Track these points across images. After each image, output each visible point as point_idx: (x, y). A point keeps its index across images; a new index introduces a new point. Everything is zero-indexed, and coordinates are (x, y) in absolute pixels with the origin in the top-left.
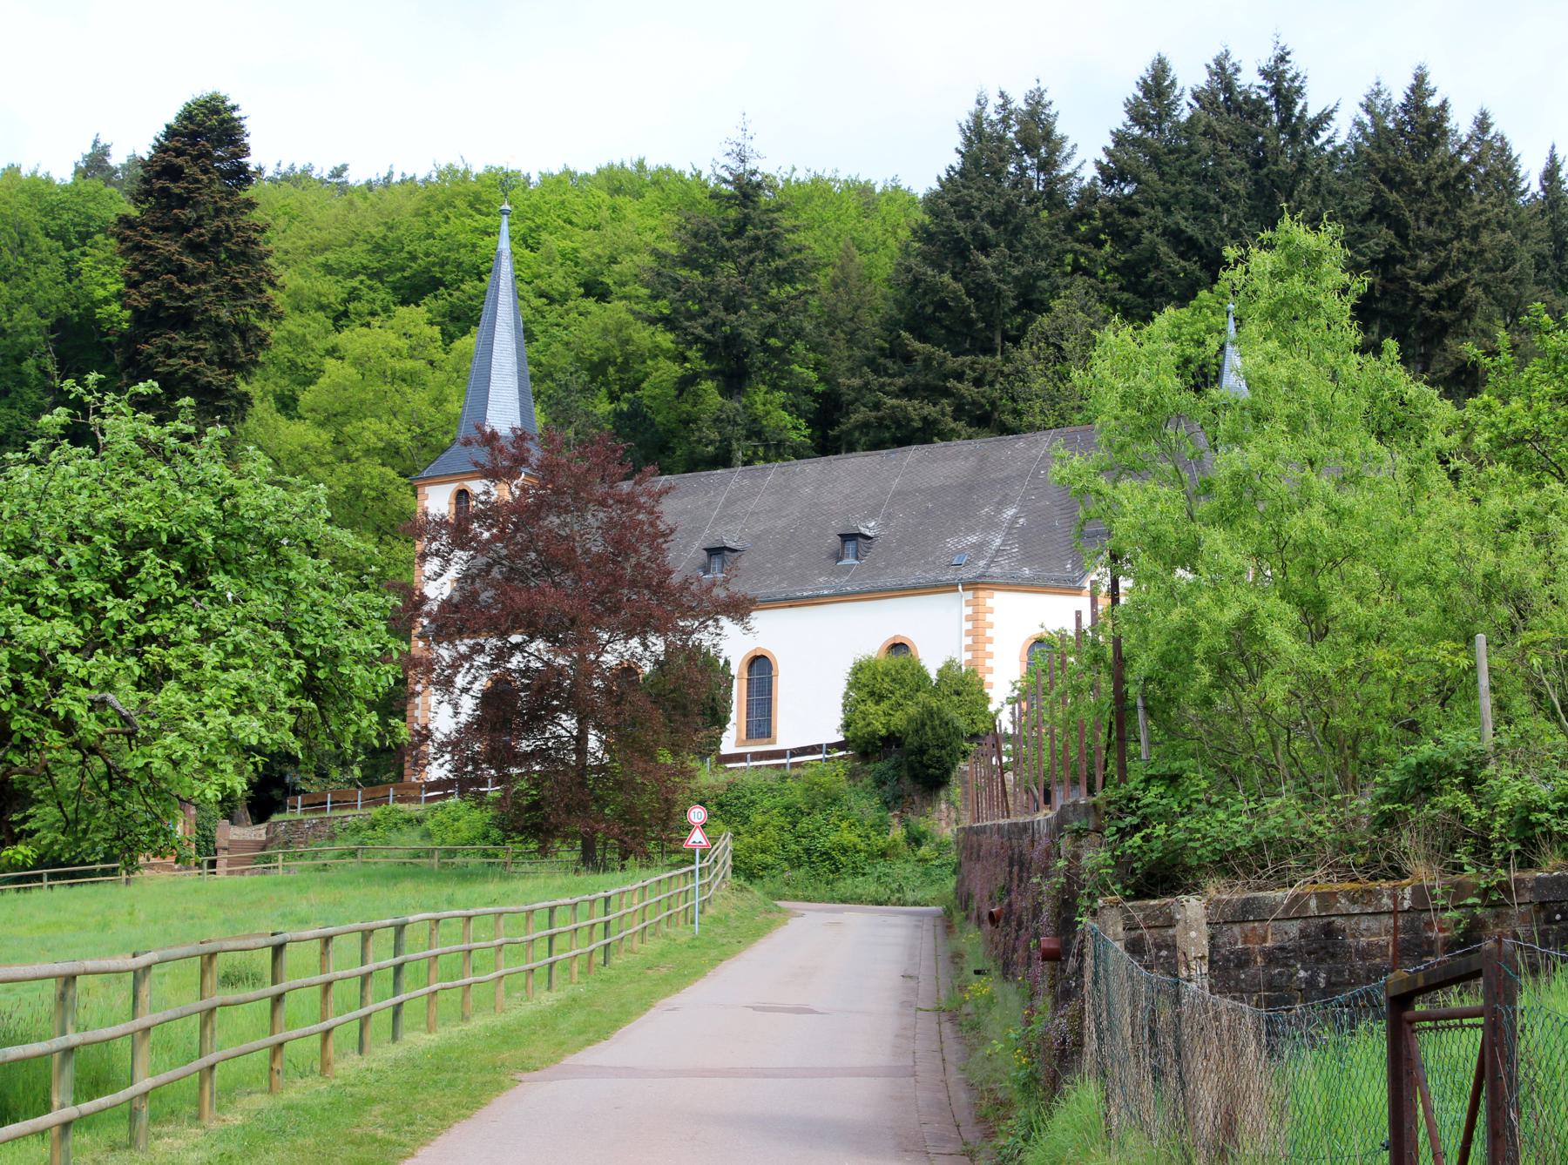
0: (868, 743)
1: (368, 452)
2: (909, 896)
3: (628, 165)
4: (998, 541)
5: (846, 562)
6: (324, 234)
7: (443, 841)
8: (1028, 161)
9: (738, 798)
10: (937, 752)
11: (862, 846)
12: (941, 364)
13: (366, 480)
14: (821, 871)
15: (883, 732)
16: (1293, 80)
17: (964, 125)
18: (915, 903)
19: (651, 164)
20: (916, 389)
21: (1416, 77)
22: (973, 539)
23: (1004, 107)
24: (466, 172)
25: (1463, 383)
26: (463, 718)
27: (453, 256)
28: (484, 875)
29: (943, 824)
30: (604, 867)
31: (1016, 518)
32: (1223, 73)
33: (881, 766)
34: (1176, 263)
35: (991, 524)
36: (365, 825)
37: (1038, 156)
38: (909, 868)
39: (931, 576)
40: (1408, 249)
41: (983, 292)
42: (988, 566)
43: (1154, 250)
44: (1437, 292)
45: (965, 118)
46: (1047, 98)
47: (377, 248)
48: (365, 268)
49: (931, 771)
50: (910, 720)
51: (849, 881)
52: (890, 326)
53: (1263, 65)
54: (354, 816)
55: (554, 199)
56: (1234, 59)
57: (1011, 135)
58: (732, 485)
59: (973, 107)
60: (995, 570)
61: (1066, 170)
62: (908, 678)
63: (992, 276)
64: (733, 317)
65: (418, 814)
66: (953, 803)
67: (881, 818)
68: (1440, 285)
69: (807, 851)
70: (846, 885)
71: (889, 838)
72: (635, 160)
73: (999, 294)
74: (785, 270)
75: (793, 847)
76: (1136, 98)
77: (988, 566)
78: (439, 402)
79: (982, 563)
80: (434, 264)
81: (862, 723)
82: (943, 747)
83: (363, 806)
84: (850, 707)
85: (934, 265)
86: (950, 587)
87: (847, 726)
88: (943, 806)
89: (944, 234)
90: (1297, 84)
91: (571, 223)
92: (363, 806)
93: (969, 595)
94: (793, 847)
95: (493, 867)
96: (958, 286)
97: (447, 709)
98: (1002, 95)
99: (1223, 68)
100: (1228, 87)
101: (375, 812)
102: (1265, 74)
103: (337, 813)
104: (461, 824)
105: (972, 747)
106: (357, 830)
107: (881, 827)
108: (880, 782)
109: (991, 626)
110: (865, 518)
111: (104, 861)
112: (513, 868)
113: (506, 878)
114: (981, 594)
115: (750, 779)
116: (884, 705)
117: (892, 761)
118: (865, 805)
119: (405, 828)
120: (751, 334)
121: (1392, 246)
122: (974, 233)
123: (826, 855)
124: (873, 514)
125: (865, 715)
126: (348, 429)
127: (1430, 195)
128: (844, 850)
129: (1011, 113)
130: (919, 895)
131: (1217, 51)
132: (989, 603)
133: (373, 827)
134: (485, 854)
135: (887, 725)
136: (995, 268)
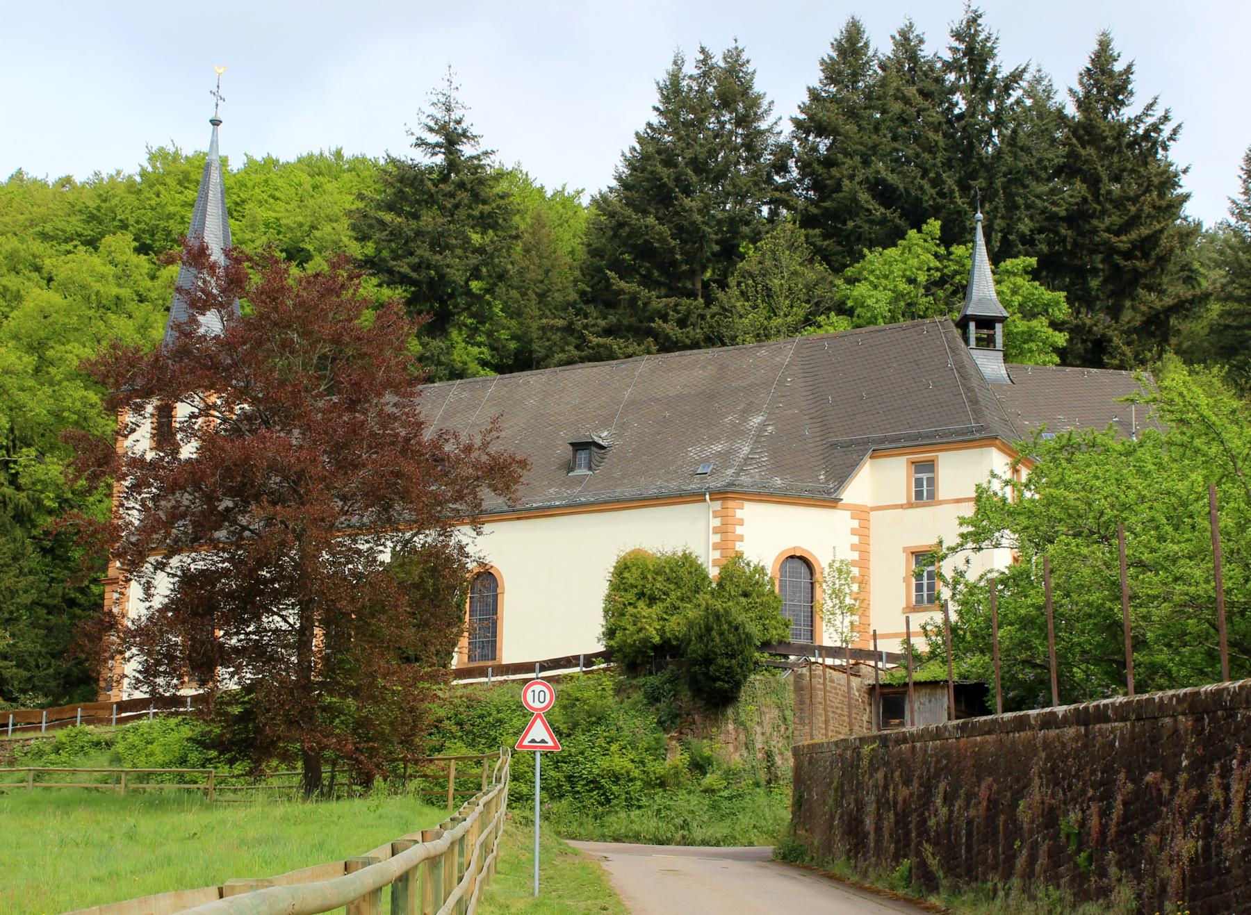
0: (639, 652)
1: (71, 377)
2: (698, 834)
3: (326, 154)
4: (746, 450)
5: (578, 472)
6: (43, 210)
7: (134, 765)
8: (726, 117)
9: (481, 717)
10: (726, 662)
11: (636, 773)
12: (645, 304)
13: (68, 402)
14: (588, 803)
15: (657, 640)
16: (987, 39)
17: (662, 83)
18: (704, 843)
19: (347, 154)
20: (619, 330)
21: (1101, 43)
22: (718, 448)
23: (704, 62)
24: (176, 153)
25: (1153, 335)
26: (157, 602)
27: (163, 224)
28: (180, 803)
29: (731, 748)
30: (328, 794)
31: (763, 425)
32: (907, 43)
33: (654, 680)
34: (879, 211)
35: (737, 432)
36: (48, 748)
37: (736, 110)
38: (694, 800)
39: (674, 485)
40: (1099, 203)
41: (688, 234)
42: (738, 474)
43: (854, 199)
44: (1132, 243)
45: (663, 77)
46: (744, 57)
47: (92, 217)
48: (80, 235)
49: (719, 684)
50: (691, 624)
51: (623, 815)
52: (592, 273)
53: (956, 26)
54: (35, 739)
55: (258, 178)
56: (918, 31)
57: (711, 89)
58: (451, 397)
59: (670, 67)
60: (744, 479)
61: (763, 125)
62: (686, 577)
63: (698, 218)
64: (438, 257)
65: (107, 736)
66: (742, 724)
67: (657, 740)
68: (1134, 235)
69: (569, 778)
70: (619, 820)
71: (668, 763)
72: (333, 149)
73: (703, 237)
74: (490, 215)
75: (552, 773)
76: (831, 58)
77: (738, 474)
78: (143, 329)
79: (730, 472)
80: (144, 231)
81: (632, 628)
82: (733, 656)
83: (47, 728)
84: (615, 611)
85: (637, 209)
86: (695, 497)
87: (610, 633)
88: (731, 727)
89: (648, 180)
90: (989, 44)
91: (276, 199)
92: (47, 728)
93: (717, 505)
94: (552, 773)
95: (191, 794)
96: (665, 230)
97: (135, 590)
98: (703, 51)
99: (907, 39)
100: (913, 57)
101: (61, 734)
102: (958, 36)
103: (19, 736)
104: (154, 747)
105: (764, 657)
106: (40, 754)
107: (658, 751)
108: (653, 698)
109: (741, 538)
110: (596, 428)
111: (995, 844)
112: (216, 795)
113: (209, 807)
114: (730, 504)
115: (496, 697)
116: (657, 609)
117: (667, 674)
118: (636, 724)
119: (92, 752)
120: (457, 275)
121: (1085, 199)
122: (677, 180)
123: (594, 784)
124: (605, 424)
125: (636, 619)
126: (50, 353)
127: (1120, 152)
128: (616, 778)
129: (712, 68)
130: (708, 832)
131: (902, 24)
132: (739, 514)
133: (57, 750)
134: (181, 778)
135: (661, 632)
136: (700, 211)
